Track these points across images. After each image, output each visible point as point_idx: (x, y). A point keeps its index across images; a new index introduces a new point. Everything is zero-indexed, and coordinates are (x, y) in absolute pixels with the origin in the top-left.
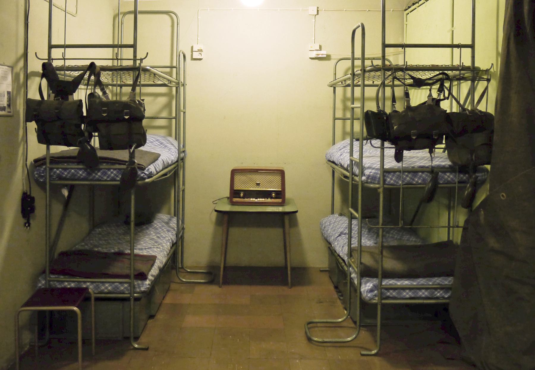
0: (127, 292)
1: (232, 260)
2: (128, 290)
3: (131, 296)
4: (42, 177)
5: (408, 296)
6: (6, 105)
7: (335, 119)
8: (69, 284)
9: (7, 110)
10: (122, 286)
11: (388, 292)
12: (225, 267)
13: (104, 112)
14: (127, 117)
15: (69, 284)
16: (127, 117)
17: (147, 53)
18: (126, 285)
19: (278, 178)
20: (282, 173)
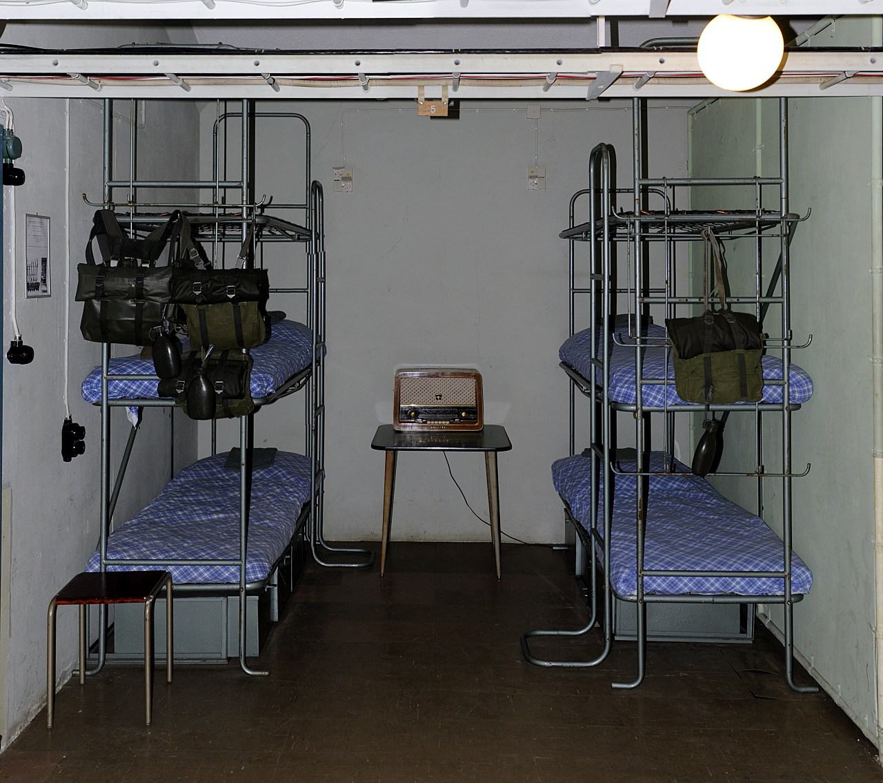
0: (234, 581)
1: (400, 532)
2: (235, 577)
3: (241, 588)
4: (96, 393)
5: (686, 590)
6: (39, 281)
7: (573, 291)
8: (751, 584)
9: (42, 288)
10: (227, 570)
11: (734, 580)
12: (388, 543)
13: (197, 289)
14: (231, 296)
15: (672, 585)
16: (231, 296)
17: (272, 198)
18: (233, 569)
19: (472, 382)
20: (478, 378)
